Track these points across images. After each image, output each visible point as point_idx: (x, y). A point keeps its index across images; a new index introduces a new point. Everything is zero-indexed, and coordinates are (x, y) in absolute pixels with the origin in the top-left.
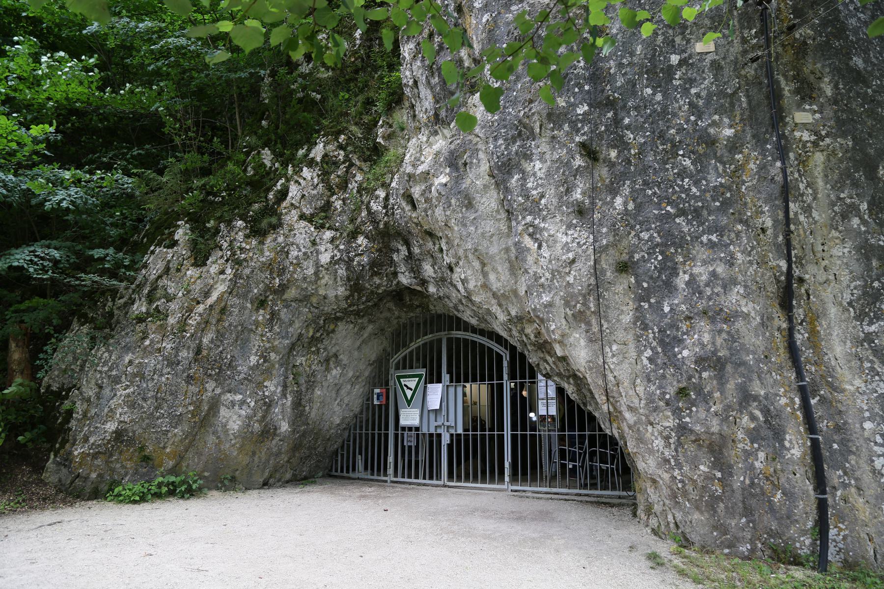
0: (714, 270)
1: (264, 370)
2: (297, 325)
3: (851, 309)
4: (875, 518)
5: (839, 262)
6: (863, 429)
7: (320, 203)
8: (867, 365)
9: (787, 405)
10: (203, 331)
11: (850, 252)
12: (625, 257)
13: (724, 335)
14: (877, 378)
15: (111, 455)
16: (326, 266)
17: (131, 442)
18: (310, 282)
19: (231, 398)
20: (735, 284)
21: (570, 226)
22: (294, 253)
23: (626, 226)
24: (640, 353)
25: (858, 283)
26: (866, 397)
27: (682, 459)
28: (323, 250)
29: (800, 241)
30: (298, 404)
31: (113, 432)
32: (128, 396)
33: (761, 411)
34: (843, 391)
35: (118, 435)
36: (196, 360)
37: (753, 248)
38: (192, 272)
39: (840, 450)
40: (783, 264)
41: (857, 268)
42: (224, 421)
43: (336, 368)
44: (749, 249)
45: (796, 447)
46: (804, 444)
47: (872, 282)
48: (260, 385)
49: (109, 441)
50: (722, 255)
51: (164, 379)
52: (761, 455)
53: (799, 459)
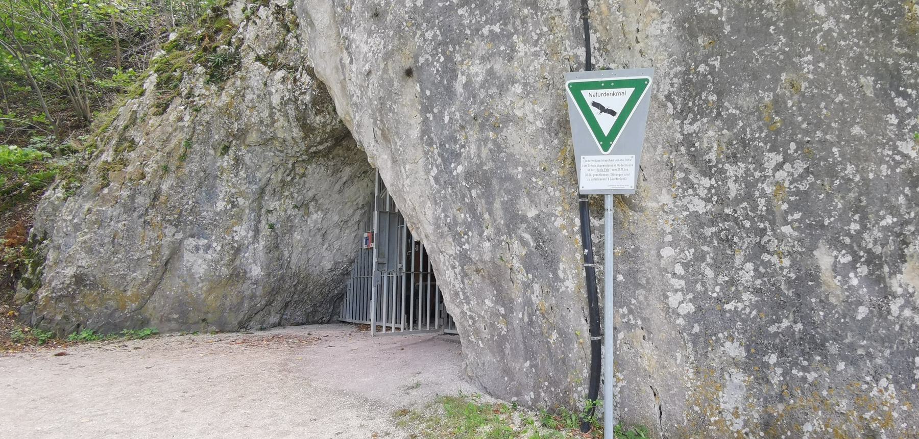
0: (491, 68)
1: (234, 213)
2: (264, 169)
3: (669, 105)
4: (664, 367)
5: (656, 43)
6: (659, 256)
7: (274, 44)
8: (680, 175)
9: (563, 227)
10: (161, 178)
11: (670, 28)
12: (408, 64)
13: (490, 145)
14: (690, 191)
15: (73, 298)
16: (278, 108)
17: (94, 285)
18: (267, 125)
19: (194, 243)
20: (513, 83)
21: (370, 33)
22: (249, 96)
23: (413, 25)
24: (427, 172)
25: (679, 68)
26: (672, 217)
27: (469, 291)
28: (274, 91)
29: (602, 21)
30: (274, 247)
31: (72, 277)
32: (85, 242)
33: (532, 235)
34: (642, 210)
35: (79, 279)
36: (153, 206)
37: (540, 35)
38: (153, 121)
39: (625, 283)
40: (581, 52)
41: (675, 47)
42: (188, 265)
43: (316, 212)
44: (536, 37)
45: (571, 280)
46: (578, 275)
47: (697, 66)
48: (229, 230)
49: (69, 285)
50: (502, 48)
51: (120, 225)
52: (536, 287)
53: (574, 292)
